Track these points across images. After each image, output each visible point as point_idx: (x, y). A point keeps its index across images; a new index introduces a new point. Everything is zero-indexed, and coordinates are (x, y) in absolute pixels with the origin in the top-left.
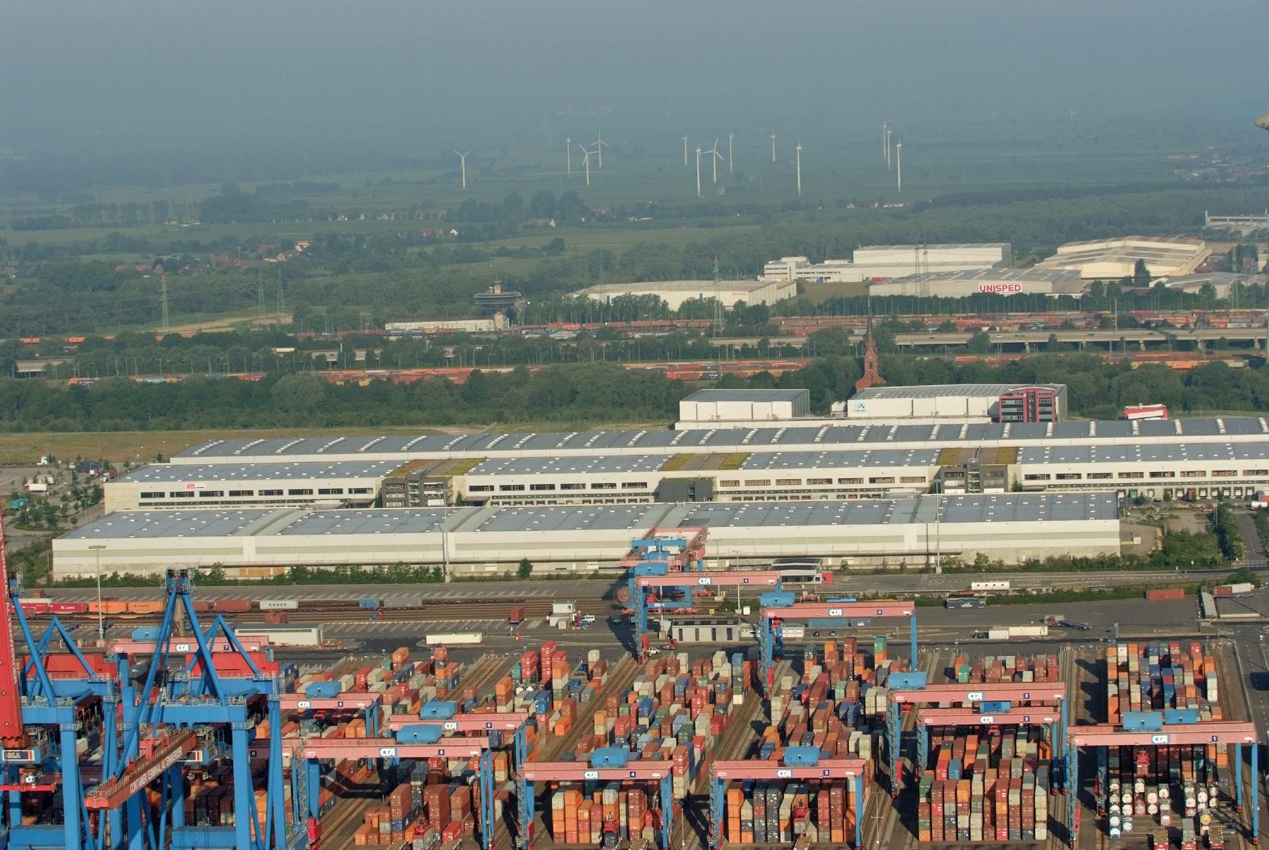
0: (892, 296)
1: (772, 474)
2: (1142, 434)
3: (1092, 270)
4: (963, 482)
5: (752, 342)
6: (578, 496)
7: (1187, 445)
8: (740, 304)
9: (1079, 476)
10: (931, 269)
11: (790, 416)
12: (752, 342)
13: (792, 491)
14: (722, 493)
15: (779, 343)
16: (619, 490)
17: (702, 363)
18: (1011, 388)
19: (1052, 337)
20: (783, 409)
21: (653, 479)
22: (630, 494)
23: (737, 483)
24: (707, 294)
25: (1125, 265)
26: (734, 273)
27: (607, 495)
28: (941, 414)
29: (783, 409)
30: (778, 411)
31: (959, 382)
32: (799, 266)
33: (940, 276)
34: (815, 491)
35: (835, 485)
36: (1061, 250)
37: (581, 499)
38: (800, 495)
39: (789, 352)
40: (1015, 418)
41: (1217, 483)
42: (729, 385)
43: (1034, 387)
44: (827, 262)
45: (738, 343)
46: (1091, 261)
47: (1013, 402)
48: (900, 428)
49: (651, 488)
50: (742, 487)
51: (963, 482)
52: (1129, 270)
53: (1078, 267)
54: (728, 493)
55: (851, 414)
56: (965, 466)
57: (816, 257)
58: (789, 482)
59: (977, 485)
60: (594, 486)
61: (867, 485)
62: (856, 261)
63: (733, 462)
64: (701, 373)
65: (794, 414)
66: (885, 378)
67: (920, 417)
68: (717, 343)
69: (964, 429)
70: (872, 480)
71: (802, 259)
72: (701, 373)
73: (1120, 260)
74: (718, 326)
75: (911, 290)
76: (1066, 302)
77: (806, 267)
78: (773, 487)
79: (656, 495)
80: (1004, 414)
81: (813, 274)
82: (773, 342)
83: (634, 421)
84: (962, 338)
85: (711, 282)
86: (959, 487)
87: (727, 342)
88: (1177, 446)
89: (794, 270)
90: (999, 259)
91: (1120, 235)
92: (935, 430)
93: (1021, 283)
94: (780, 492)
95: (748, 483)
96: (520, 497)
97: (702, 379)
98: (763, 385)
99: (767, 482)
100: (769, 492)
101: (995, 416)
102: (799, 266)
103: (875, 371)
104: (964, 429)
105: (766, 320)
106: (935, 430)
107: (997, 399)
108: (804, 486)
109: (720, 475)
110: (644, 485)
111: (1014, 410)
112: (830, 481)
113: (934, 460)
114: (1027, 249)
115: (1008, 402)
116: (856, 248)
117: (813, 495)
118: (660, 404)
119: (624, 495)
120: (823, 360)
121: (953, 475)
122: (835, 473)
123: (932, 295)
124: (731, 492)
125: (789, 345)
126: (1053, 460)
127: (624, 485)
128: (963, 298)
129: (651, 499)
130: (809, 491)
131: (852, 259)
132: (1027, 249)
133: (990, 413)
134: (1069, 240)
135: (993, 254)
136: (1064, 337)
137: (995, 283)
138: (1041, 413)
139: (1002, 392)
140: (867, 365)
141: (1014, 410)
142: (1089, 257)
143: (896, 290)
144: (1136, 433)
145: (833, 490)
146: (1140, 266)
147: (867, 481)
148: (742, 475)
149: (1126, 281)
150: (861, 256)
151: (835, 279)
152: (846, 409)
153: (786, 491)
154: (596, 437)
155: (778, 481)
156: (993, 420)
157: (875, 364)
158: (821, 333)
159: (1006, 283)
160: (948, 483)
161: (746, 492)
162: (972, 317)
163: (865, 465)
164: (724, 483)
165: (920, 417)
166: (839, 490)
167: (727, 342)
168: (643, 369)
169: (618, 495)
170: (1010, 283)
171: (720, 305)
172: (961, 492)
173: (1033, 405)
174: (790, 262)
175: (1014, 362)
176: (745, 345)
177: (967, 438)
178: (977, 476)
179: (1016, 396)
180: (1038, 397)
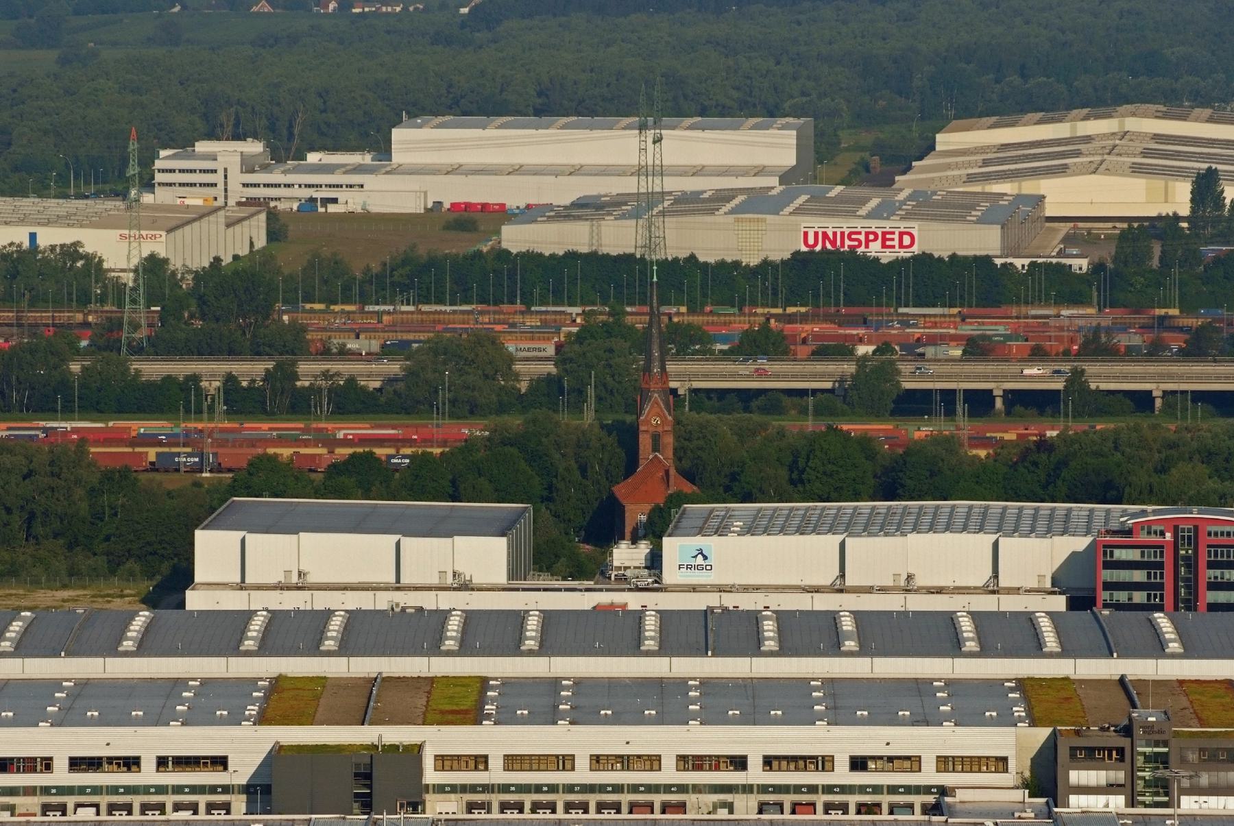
0: (572, 256)
1: (582, 740)
2: (785, 650)
3: (1067, 195)
4: (1120, 776)
5: (251, 370)
6: (30, 791)
7: (950, 683)
8: (153, 266)
9: (47, 764)
10: (673, 184)
11: (502, 578)
12: (251, 370)
13: (634, 788)
14: (440, 789)
15: (326, 375)
16: (148, 775)
17: (140, 426)
18: (1121, 513)
19: (1077, 374)
20: (485, 557)
21: (247, 746)
22: (178, 789)
23: (480, 762)
24: (49, 237)
25: (1158, 183)
26: (63, 180)
27: (114, 790)
28: (920, 581)
29: (485, 557)
30: (471, 562)
31: (890, 493)
32: (248, 166)
33: (689, 203)
34: (697, 789)
35: (755, 774)
36: (945, 141)
37: (753, 800)
38: (658, 799)
39: (349, 400)
40: (1139, 597)
41: (779, 789)
42: (357, 488)
43: (1195, 513)
44: (313, 158)
45: (211, 373)
46: (1062, 170)
47: (1133, 555)
48: (354, 617)
49: (242, 771)
50: (496, 774)
51: (1120, 776)
52: (1178, 199)
53: (1030, 187)
54: (454, 789)
55: (670, 575)
56: (1127, 731)
57: (286, 147)
58: (625, 762)
59: (1162, 786)
60: (77, 764)
61: (842, 775)
62: (397, 158)
63: (464, 704)
64: (152, 453)
65: (513, 573)
66: (689, 475)
67: (869, 590)
68: (152, 369)
69: (336, 624)
70: (858, 764)
71: (254, 147)
72: (152, 453)
73: (1137, 170)
74: (136, 327)
75: (618, 237)
76: (1055, 284)
77: (265, 168)
78: (582, 774)
79: (248, 789)
80: (1109, 586)
81: (290, 186)
82: (308, 371)
83: (36, 583)
84: (821, 376)
85: (113, 206)
86: (1111, 788)
87: (180, 368)
88: (803, 684)
89: (237, 178)
90: (789, 159)
91: (1101, 101)
92: (256, 626)
93: (915, 227)
94: (602, 788)
95: (512, 762)
96: (909, 790)
97: (153, 467)
98: (435, 488)
99: (565, 762)
100: (570, 789)
101: (1079, 590)
102: (248, 166)
103: (666, 457)
104: (336, 624)
105: (266, 311)
106: (256, 626)
107: (1081, 543)
108: (669, 774)
109: (438, 740)
110: (220, 762)
111: (1139, 576)
112: (740, 763)
113: (253, 710)
114: (868, 136)
115: (1121, 555)
116: (397, 123)
117: (691, 799)
118: (132, 547)
119: (161, 790)
120: (515, 422)
121: (1090, 756)
122: (755, 741)
123: (683, 254)
124: (464, 789)
125: (351, 380)
126: (839, 715)
127: (162, 762)
128: (766, 263)
129: (239, 804)
130: (682, 789)
131: (383, 149)
132: (868, 136)
133: (1059, 584)
134: (972, 109)
135: (773, 147)
136: (1105, 377)
137: (844, 225)
138: (1215, 586)
139: (1098, 523)
140: (645, 441)
141: (1139, 576)
142: (1057, 160)
143: (574, 237)
144: (770, 645)
145: (747, 789)
146: (1206, 188)
147: (842, 764)
148: (493, 739)
149: (1163, 227)
150: (412, 142)
151: (350, 202)
152: (654, 562)
153: (618, 789)
154: (17, 626)
155: (682, 759)
156: (1073, 604)
157: (669, 440)
158: (441, 351)
159: (874, 225)
160: (1076, 777)
161: (505, 788)
162: (804, 318)
163: (58, 722)
164: (443, 762)
165: (869, 590)
166: (764, 789)
167: (180, 368)
168: (1002, 439)
169: (146, 790)
170: (887, 225)
171: (94, 265)
172: (1117, 802)
173: (1191, 563)
174: (227, 154)
175: (1043, 445)
176: (230, 379)
177: (346, 648)
178: (1161, 760)
179: (1143, 537)
180: (1204, 541)
